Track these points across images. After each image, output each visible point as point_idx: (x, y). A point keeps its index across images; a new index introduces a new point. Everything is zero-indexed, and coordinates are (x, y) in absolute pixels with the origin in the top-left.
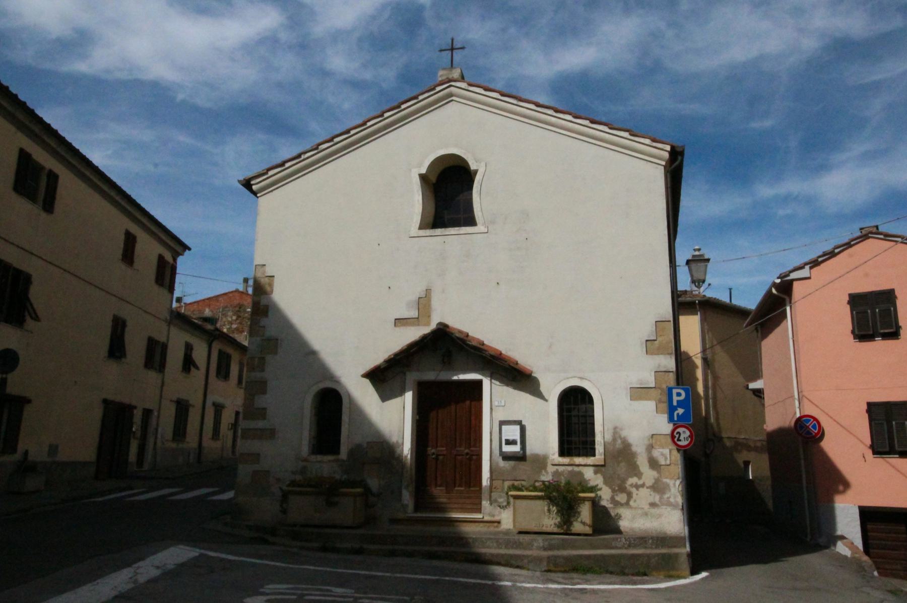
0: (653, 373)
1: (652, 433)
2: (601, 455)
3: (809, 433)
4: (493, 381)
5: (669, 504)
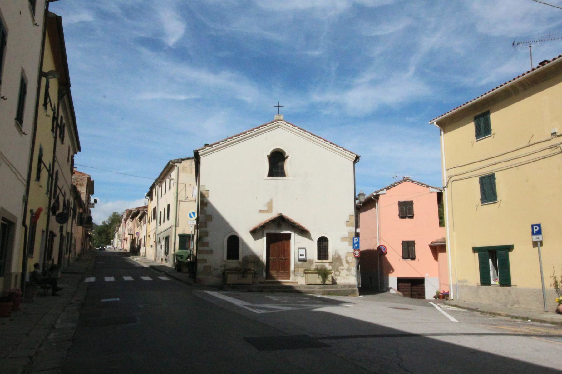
0: (348, 232)
1: (348, 252)
2: (331, 259)
3: (382, 251)
4: (295, 234)
5: (352, 275)
